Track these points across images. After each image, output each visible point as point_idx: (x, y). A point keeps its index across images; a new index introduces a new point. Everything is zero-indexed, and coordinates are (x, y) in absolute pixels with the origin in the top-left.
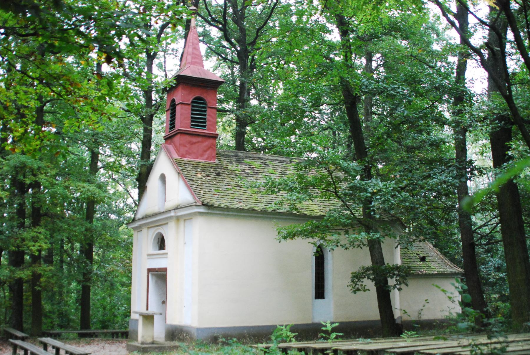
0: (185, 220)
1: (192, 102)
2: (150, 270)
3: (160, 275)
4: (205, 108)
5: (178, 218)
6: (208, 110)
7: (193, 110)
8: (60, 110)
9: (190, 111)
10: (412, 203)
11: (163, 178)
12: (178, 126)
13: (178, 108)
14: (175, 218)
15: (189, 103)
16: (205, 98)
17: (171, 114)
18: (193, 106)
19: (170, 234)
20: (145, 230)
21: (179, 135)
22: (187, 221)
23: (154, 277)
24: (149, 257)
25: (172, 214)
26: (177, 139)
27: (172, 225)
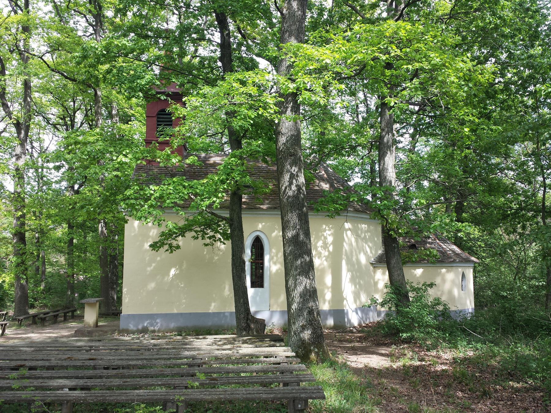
1: (158, 114)
7: (158, 121)
18: (158, 118)
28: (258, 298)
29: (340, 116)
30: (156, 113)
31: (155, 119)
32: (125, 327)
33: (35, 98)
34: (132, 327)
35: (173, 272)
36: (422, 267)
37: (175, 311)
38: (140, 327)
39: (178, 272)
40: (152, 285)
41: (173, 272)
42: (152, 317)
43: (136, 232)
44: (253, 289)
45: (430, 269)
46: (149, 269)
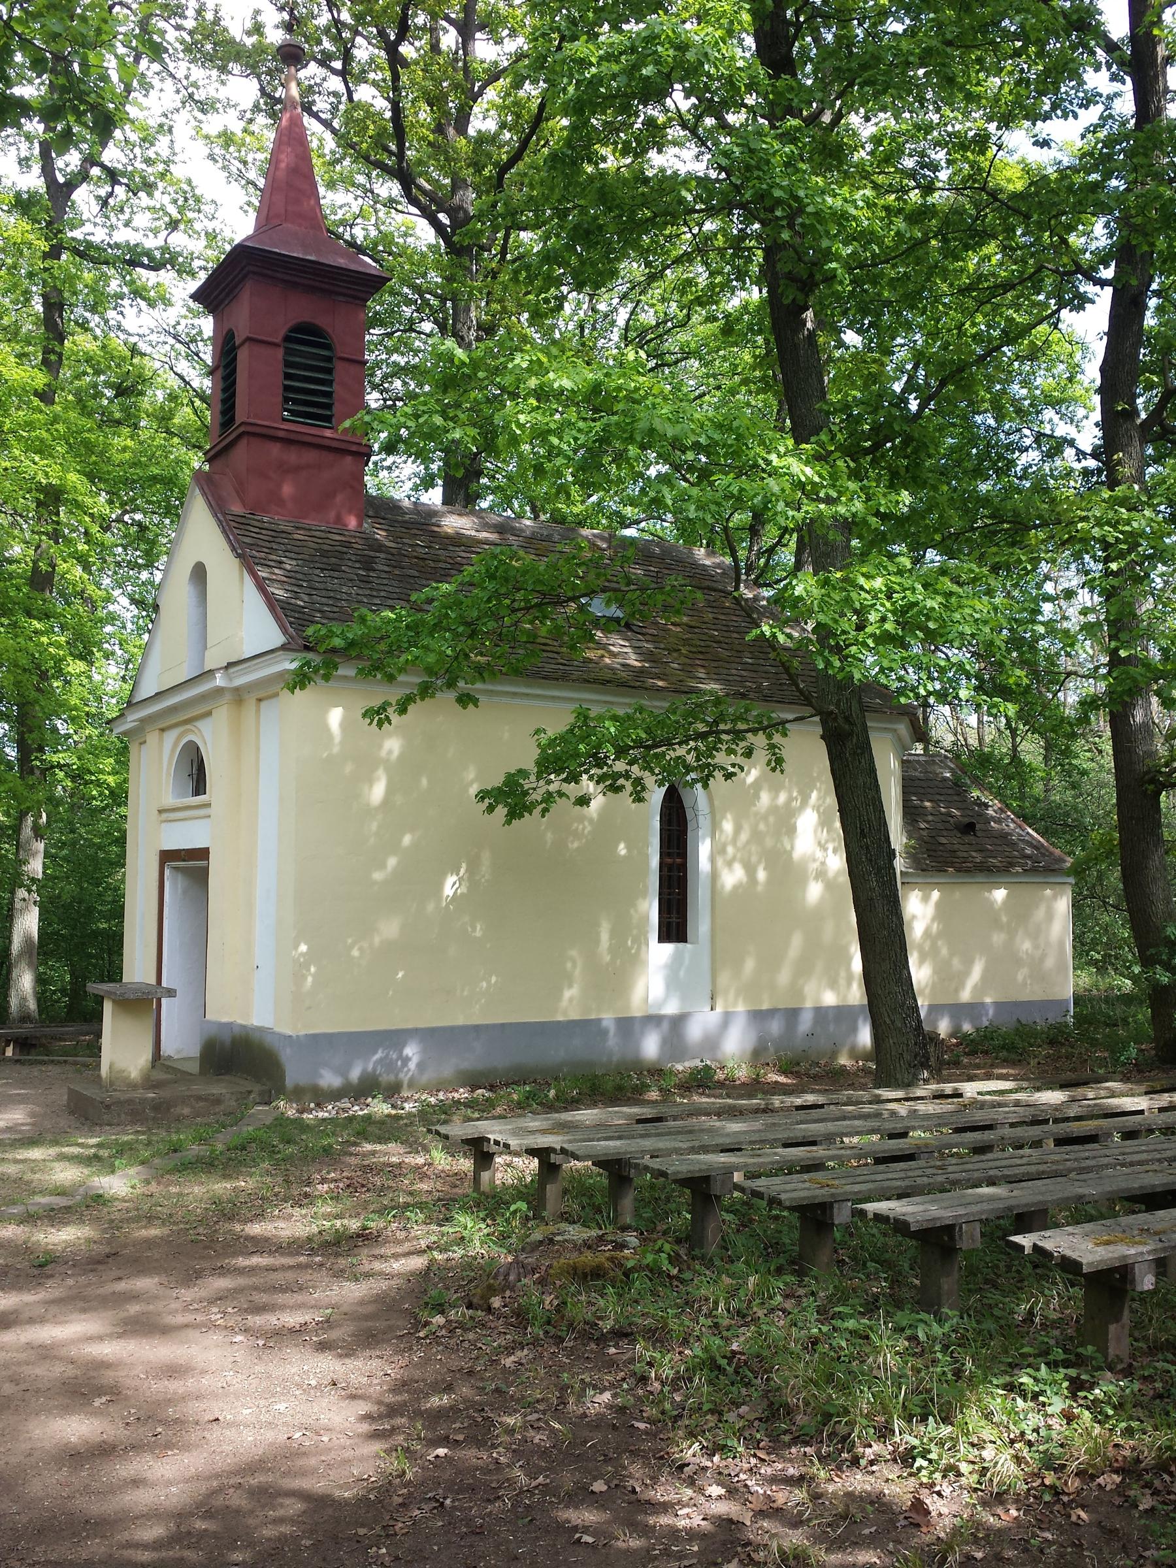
0: (260, 700)
1: (287, 339)
2: (167, 857)
3: (190, 865)
4: (329, 359)
5: (238, 696)
6: (339, 367)
7: (288, 364)
8: (640, 1202)
9: (281, 366)
10: (1133, 1449)
11: (199, 573)
12: (240, 416)
13: (243, 356)
14: (228, 697)
15: (278, 340)
16: (330, 330)
17: (225, 379)
18: (288, 351)
19: (213, 738)
20: (152, 738)
21: (244, 442)
22: (263, 704)
23: (180, 877)
24: (164, 816)
25: (219, 680)
26: (241, 454)
27: (222, 714)
28: (682, 973)
29: (758, 352)
30: (282, 332)
31: (280, 353)
32: (303, 1081)
33: (1148, 728)
34: (330, 1079)
35: (450, 886)
36: (1006, 885)
37: (460, 1021)
38: (355, 1074)
39: (463, 890)
40: (390, 929)
41: (450, 886)
42: (395, 1038)
43: (336, 750)
44: (669, 948)
45: (958, 894)
46: (378, 876)
